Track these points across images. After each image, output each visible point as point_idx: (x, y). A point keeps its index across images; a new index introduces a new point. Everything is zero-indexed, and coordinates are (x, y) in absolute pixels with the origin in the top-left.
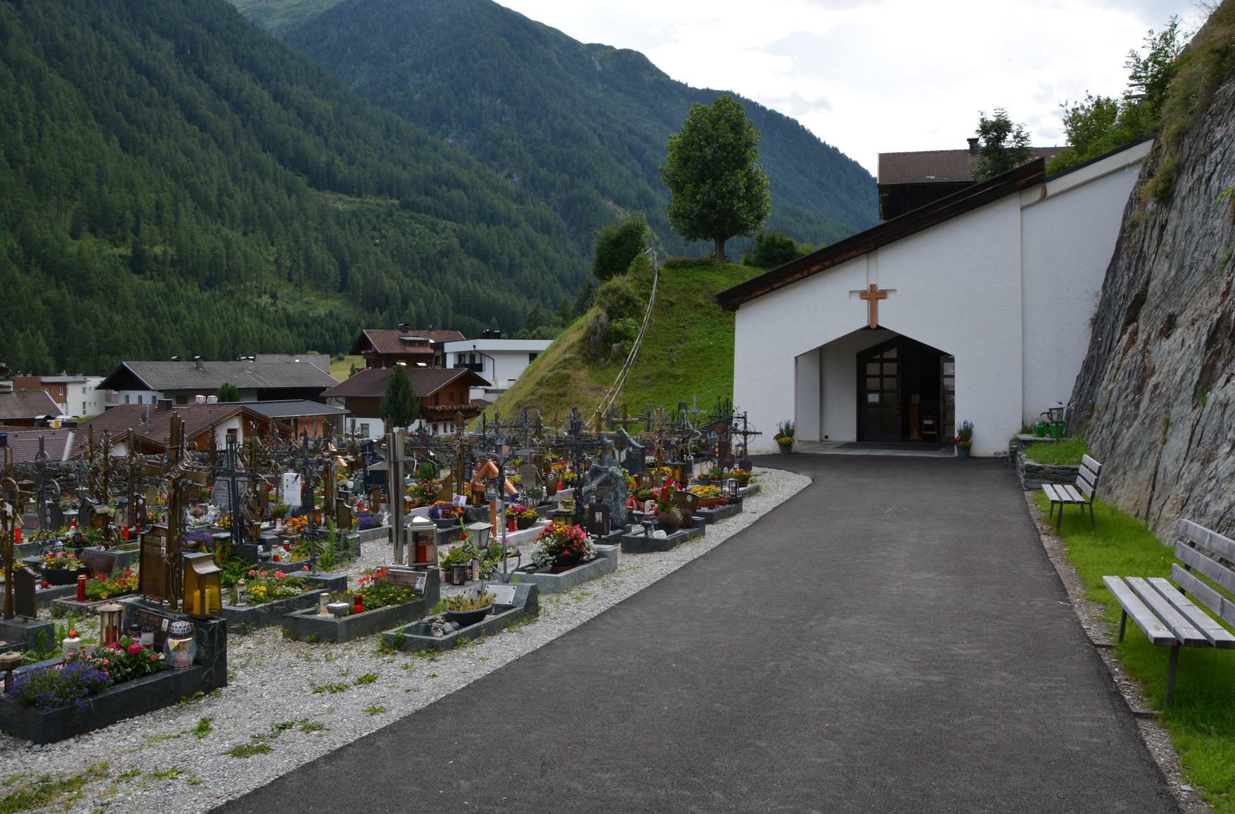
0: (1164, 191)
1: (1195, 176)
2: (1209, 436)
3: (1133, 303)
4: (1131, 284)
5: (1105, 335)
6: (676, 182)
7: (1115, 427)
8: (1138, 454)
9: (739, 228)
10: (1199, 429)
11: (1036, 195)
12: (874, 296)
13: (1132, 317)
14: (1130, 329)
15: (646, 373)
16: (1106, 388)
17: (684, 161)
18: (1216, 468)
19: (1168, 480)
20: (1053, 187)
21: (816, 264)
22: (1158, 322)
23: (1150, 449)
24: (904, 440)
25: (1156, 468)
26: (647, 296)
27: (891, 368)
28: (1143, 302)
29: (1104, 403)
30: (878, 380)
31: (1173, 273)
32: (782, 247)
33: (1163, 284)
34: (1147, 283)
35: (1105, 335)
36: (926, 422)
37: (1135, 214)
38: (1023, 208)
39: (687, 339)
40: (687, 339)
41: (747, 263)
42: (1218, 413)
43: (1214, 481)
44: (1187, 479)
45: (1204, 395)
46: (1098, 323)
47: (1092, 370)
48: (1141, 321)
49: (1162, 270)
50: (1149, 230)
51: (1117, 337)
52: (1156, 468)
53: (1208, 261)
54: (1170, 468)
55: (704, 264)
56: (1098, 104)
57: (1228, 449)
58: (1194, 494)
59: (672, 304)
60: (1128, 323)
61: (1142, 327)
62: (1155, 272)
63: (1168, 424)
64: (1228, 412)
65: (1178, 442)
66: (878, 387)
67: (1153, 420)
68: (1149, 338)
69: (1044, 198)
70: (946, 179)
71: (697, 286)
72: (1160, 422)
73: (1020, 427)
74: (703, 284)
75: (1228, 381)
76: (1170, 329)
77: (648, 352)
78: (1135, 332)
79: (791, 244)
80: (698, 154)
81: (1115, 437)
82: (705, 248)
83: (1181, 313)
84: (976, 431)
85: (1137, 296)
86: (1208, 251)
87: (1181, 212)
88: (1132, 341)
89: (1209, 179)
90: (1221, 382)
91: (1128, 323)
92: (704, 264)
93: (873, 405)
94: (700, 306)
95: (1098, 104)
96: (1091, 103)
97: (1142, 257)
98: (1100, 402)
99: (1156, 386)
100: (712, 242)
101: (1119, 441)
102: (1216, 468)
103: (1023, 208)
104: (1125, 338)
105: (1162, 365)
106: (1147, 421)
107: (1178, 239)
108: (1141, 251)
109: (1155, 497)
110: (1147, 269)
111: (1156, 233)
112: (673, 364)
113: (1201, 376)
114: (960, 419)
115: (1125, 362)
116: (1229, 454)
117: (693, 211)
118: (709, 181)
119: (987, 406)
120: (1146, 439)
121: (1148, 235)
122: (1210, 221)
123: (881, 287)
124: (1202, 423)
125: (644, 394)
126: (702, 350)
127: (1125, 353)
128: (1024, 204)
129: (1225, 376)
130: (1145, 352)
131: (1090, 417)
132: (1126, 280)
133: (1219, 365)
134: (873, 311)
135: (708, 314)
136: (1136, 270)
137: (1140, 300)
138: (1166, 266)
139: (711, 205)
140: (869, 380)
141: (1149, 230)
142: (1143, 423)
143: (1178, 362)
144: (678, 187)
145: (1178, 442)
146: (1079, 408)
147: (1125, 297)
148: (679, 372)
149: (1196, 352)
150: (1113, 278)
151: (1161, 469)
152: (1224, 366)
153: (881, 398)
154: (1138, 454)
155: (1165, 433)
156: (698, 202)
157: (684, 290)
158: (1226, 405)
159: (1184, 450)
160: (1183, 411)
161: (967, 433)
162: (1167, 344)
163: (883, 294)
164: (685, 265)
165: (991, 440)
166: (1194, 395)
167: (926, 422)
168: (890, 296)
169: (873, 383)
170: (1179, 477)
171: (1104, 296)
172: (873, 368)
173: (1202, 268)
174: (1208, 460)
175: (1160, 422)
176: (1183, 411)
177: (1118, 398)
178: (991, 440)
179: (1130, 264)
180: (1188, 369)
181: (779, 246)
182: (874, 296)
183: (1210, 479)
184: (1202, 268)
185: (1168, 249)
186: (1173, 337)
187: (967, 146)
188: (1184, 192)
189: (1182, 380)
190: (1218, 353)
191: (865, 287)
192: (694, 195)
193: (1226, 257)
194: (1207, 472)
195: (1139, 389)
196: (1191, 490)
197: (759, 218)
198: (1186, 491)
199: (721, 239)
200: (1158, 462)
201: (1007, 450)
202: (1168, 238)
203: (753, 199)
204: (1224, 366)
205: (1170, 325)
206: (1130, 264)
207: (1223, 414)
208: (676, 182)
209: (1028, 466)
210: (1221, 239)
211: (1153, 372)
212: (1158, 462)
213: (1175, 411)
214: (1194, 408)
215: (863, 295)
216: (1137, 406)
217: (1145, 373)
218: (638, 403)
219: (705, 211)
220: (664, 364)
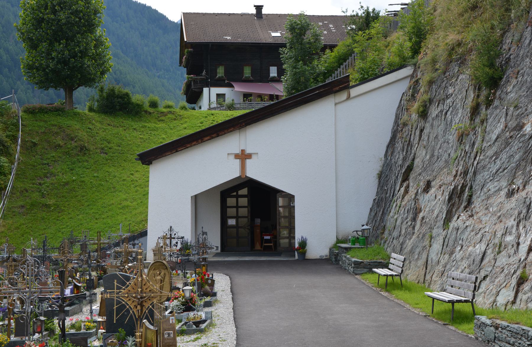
0: (423, 112)
1: (439, 109)
2: (451, 243)
3: (406, 170)
4: (404, 159)
5: (389, 186)
6: (31, 39)
7: (401, 239)
8: (417, 253)
9: (87, 80)
10: (446, 240)
11: (343, 96)
12: (243, 157)
13: (406, 178)
14: (405, 185)
15: (21, 203)
16: (393, 217)
17: (39, 22)
18: (456, 256)
19: (433, 264)
20: (354, 92)
21: (206, 136)
22: (422, 184)
23: (423, 250)
24: (251, 250)
25: (427, 258)
26: (14, 139)
27: (244, 201)
28: (411, 170)
29: (393, 226)
30: (235, 209)
31: (428, 157)
32: (121, 97)
33: (423, 162)
34: (413, 160)
35: (389, 186)
36: (266, 237)
37: (405, 117)
38: (336, 104)
39: (53, 174)
40: (53, 174)
41: (91, 109)
42: (455, 232)
43: (455, 262)
44: (443, 262)
45: (448, 224)
46: (383, 177)
47: (381, 205)
48: (411, 180)
49: (421, 156)
50: (414, 130)
51: (398, 188)
52: (427, 258)
53: (446, 156)
54: (434, 258)
55: (59, 111)
56: (368, 13)
57: (460, 248)
58: (447, 268)
59: (35, 144)
60: (403, 181)
61: (411, 184)
62: (418, 154)
63: (431, 237)
64: (459, 232)
65: (437, 246)
66: (235, 215)
67: (424, 235)
68: (417, 192)
69: (349, 98)
70: (240, 40)
71: (55, 129)
72: (427, 236)
73: (335, 239)
74: (60, 128)
75: (458, 218)
76: (428, 188)
77: (20, 185)
78: (408, 187)
79: (127, 95)
80: (52, 16)
81: (402, 244)
82: (54, 96)
83: (434, 180)
84: (308, 242)
85: (408, 166)
86: (446, 151)
87: (432, 125)
88: (406, 192)
89: (446, 113)
90: (455, 218)
91: (403, 181)
92: (59, 111)
93: (232, 227)
94: (59, 146)
95: (368, 13)
96: (362, 11)
97: (410, 144)
98: (389, 225)
99: (423, 218)
100: (62, 92)
101: (404, 246)
102: (456, 256)
103: (336, 104)
104: (403, 189)
105: (425, 207)
106: (421, 236)
107: (430, 140)
108: (410, 141)
109: (427, 272)
110: (413, 152)
111: (418, 133)
112: (43, 196)
113: (446, 215)
114: (298, 236)
115: (403, 203)
116: (460, 250)
117: (48, 66)
118: (63, 41)
119: (315, 227)
120: (421, 245)
121: (413, 132)
122: (447, 136)
123: (248, 151)
124: (448, 237)
125: (22, 221)
126: (67, 184)
127: (403, 198)
128: (337, 101)
129: (456, 216)
130: (416, 200)
131: (383, 233)
132: (401, 157)
133: (454, 210)
134: (243, 167)
135: (67, 153)
136: (407, 151)
137: (410, 169)
138: (424, 152)
139: (64, 62)
140: (228, 209)
141: (414, 130)
142: (418, 237)
143: (434, 206)
144: (33, 45)
145: (437, 246)
146: (375, 228)
147: (401, 166)
148: (51, 202)
149: (444, 204)
150: (392, 153)
151: (429, 259)
152: (456, 211)
153: (237, 222)
154: (417, 253)
155: (430, 241)
156: (53, 59)
157: (44, 133)
158: (458, 229)
159: (440, 249)
160: (438, 232)
161: (303, 244)
162: (427, 196)
163: (249, 156)
164: (42, 110)
165: (318, 249)
166: (444, 224)
167: (266, 237)
168: (254, 157)
169: (231, 212)
170: (439, 262)
171: (385, 162)
172: (231, 201)
173: (443, 159)
174: (452, 253)
175: (427, 236)
176: (438, 232)
177: (402, 223)
178: (318, 249)
179: (403, 147)
180: (440, 212)
181: (119, 97)
182: (243, 157)
183: (453, 261)
184: (443, 159)
185: (425, 143)
186: (430, 193)
187: (254, 11)
188: (434, 115)
189: (437, 217)
190: (453, 205)
191: (238, 151)
192: (49, 54)
193: (455, 157)
194: (452, 258)
195: (414, 219)
196: (445, 266)
197: (103, 73)
198: (443, 267)
199: (70, 90)
200: (428, 256)
201: (328, 254)
202: (425, 137)
203: (99, 59)
204: (456, 211)
205: (428, 186)
206: (403, 147)
207: (457, 233)
208: (31, 39)
209: (355, 262)
210: (452, 146)
211: (420, 211)
212: (428, 256)
213: (435, 232)
214: (444, 230)
215: (237, 156)
216: (414, 228)
217: (417, 211)
218: (17, 228)
219: (59, 66)
220: (36, 196)
